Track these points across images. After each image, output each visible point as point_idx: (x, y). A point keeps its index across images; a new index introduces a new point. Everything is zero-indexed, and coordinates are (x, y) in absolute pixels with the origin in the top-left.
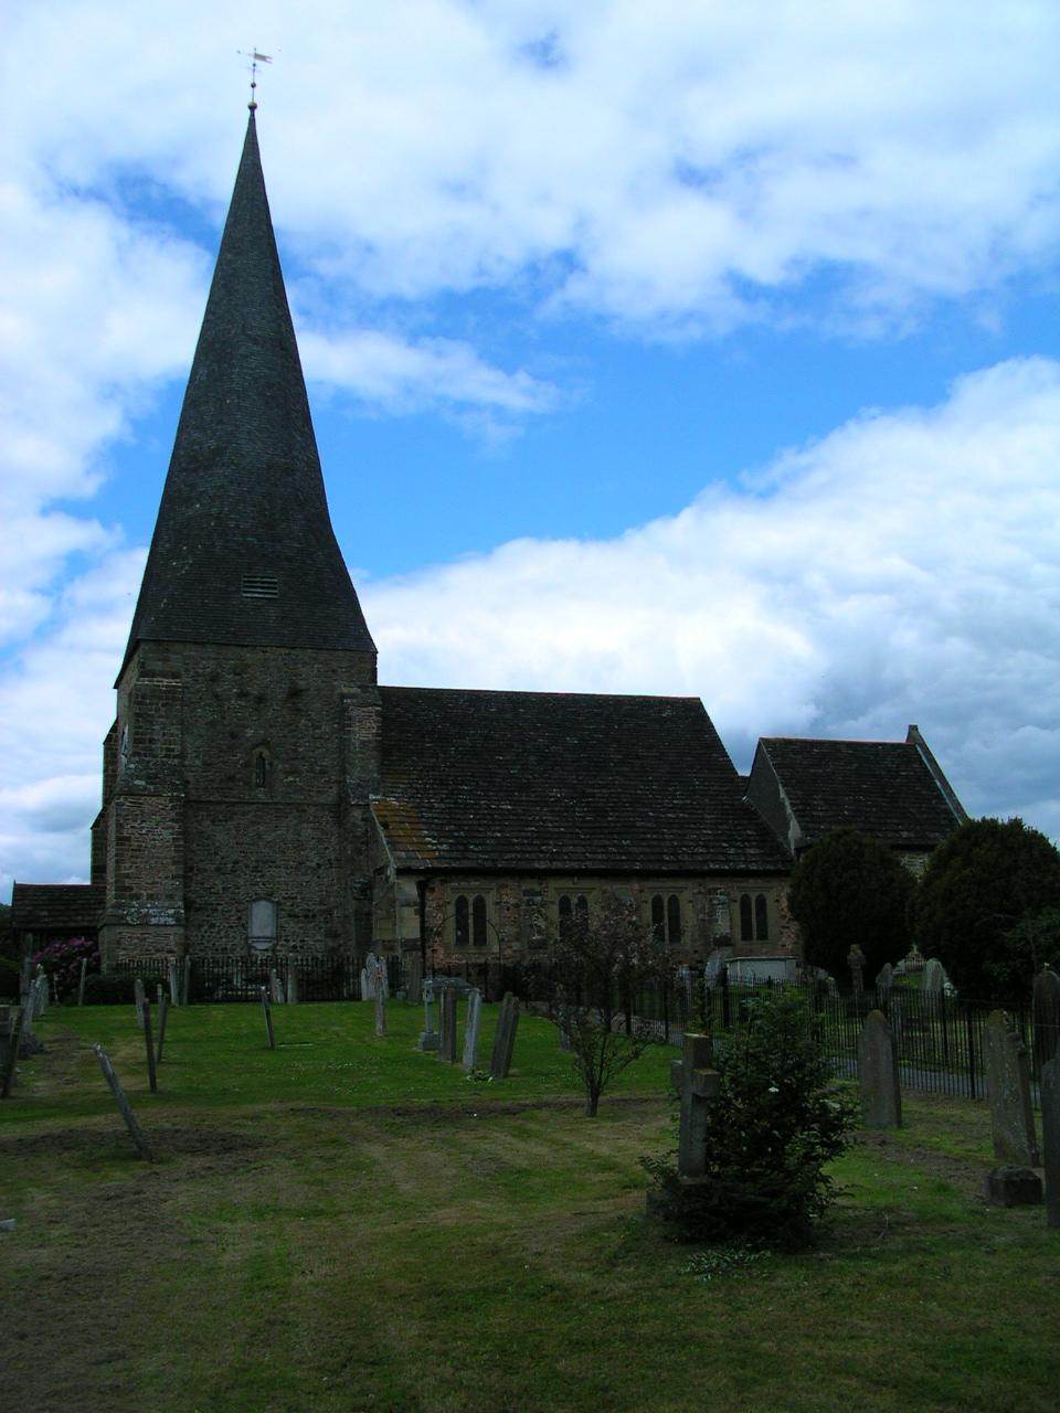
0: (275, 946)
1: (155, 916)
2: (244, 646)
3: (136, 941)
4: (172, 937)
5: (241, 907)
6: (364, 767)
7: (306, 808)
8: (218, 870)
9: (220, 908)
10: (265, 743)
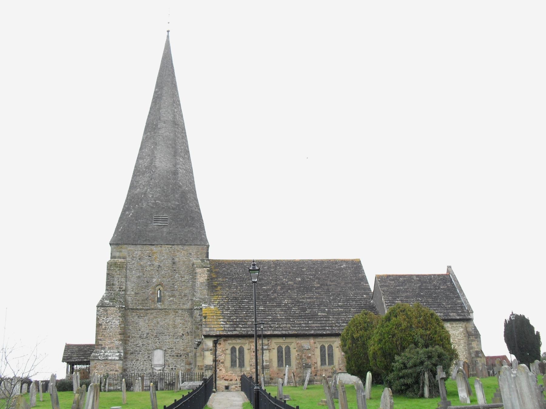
0: (163, 368)
1: (110, 356)
4: (117, 365)
5: (150, 352)
6: (201, 292)
7: (177, 310)
8: (140, 337)
9: (141, 353)
10: (160, 284)
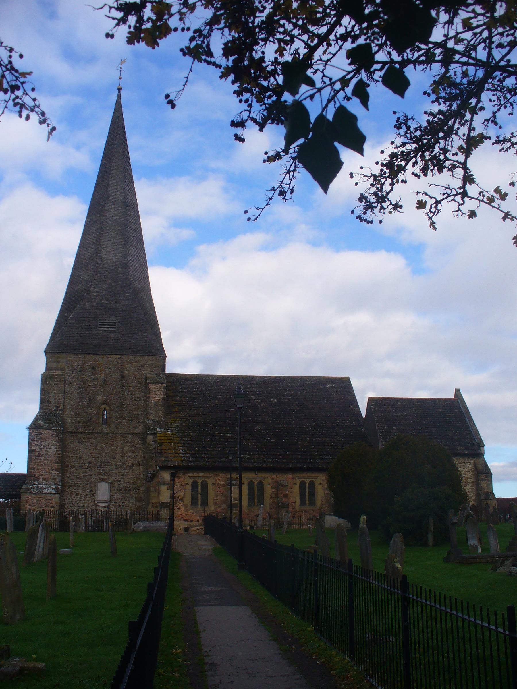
1: (45, 489)
2: (98, 354)
3: (35, 501)
5: (93, 485)
7: (126, 435)
8: (81, 466)
9: (81, 485)
